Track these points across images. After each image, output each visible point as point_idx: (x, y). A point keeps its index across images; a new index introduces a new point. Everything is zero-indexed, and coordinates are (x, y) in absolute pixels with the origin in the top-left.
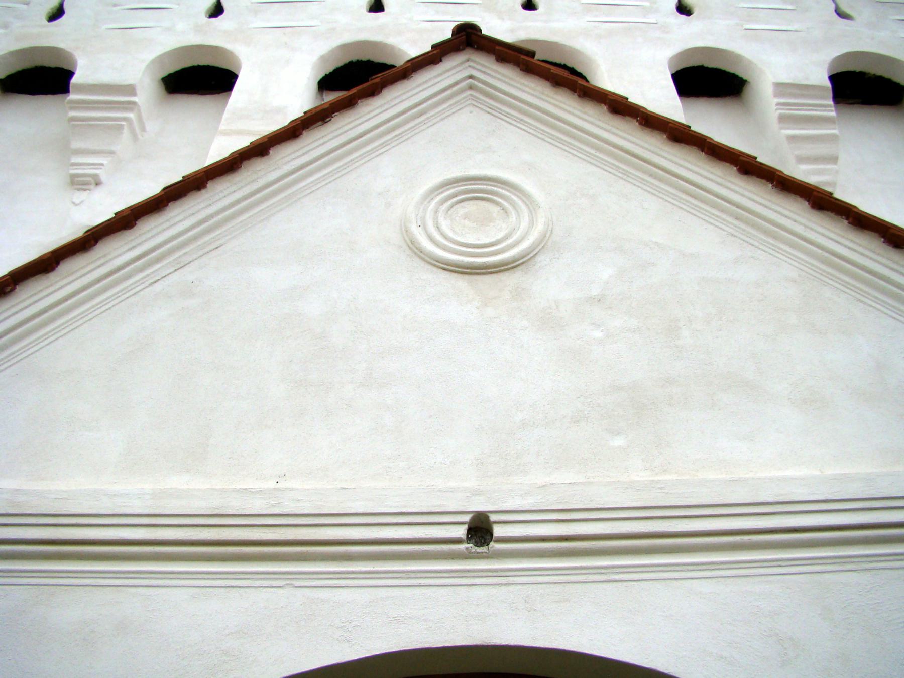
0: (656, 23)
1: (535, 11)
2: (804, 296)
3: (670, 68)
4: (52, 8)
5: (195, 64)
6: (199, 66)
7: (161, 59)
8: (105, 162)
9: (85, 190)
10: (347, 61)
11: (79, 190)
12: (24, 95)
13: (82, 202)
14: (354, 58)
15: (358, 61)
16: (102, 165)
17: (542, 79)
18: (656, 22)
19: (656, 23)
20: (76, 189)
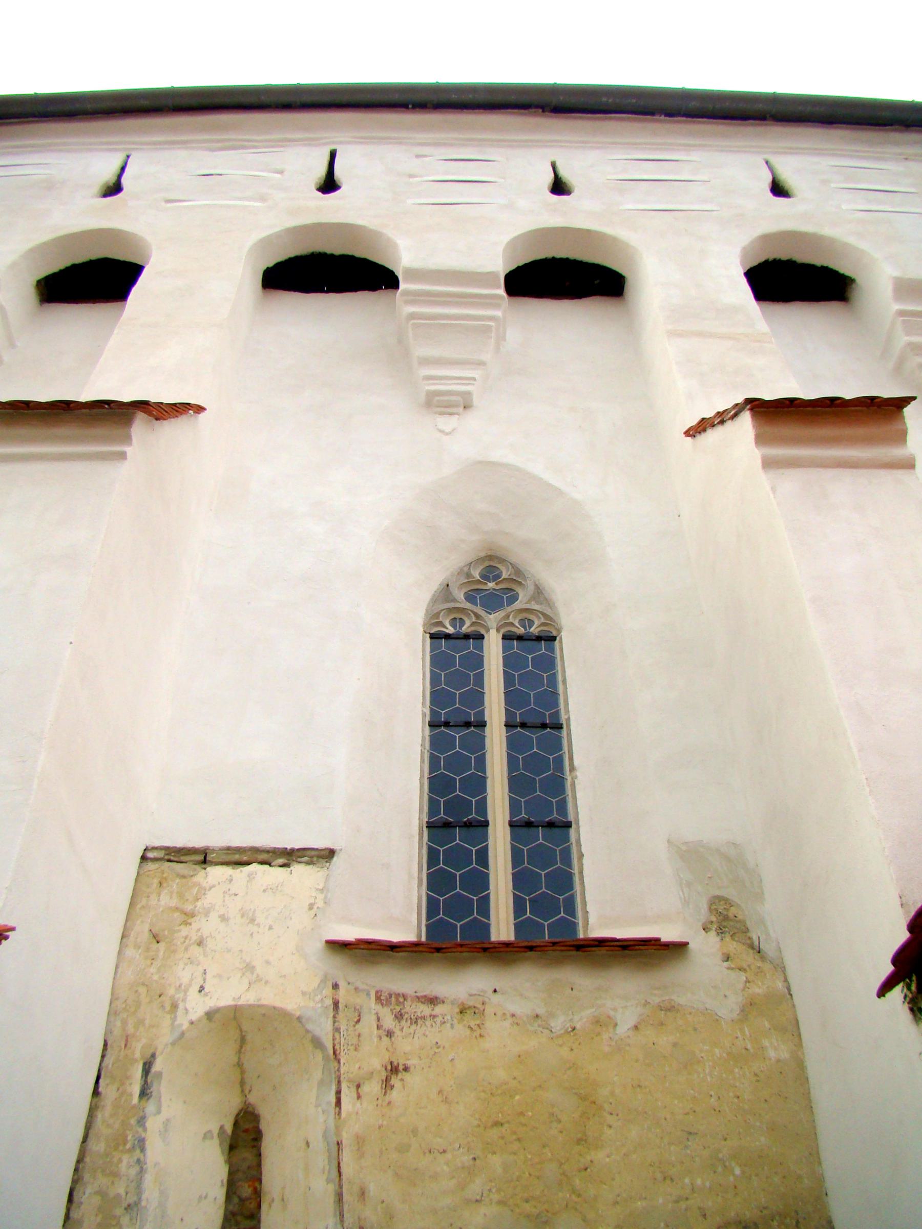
0: (709, 181)
1: (789, 199)
2: (711, 1165)
3: (742, 264)
4: (320, 178)
5: (549, 255)
6: (554, 259)
7: (265, 244)
8: (476, 376)
9: (451, 414)
10: (762, 259)
11: (442, 414)
12: (66, 305)
13: (454, 430)
14: (771, 257)
15: (775, 260)
16: (474, 379)
17: (39, 297)
18: (708, 180)
19: (709, 181)
20: (436, 413)
